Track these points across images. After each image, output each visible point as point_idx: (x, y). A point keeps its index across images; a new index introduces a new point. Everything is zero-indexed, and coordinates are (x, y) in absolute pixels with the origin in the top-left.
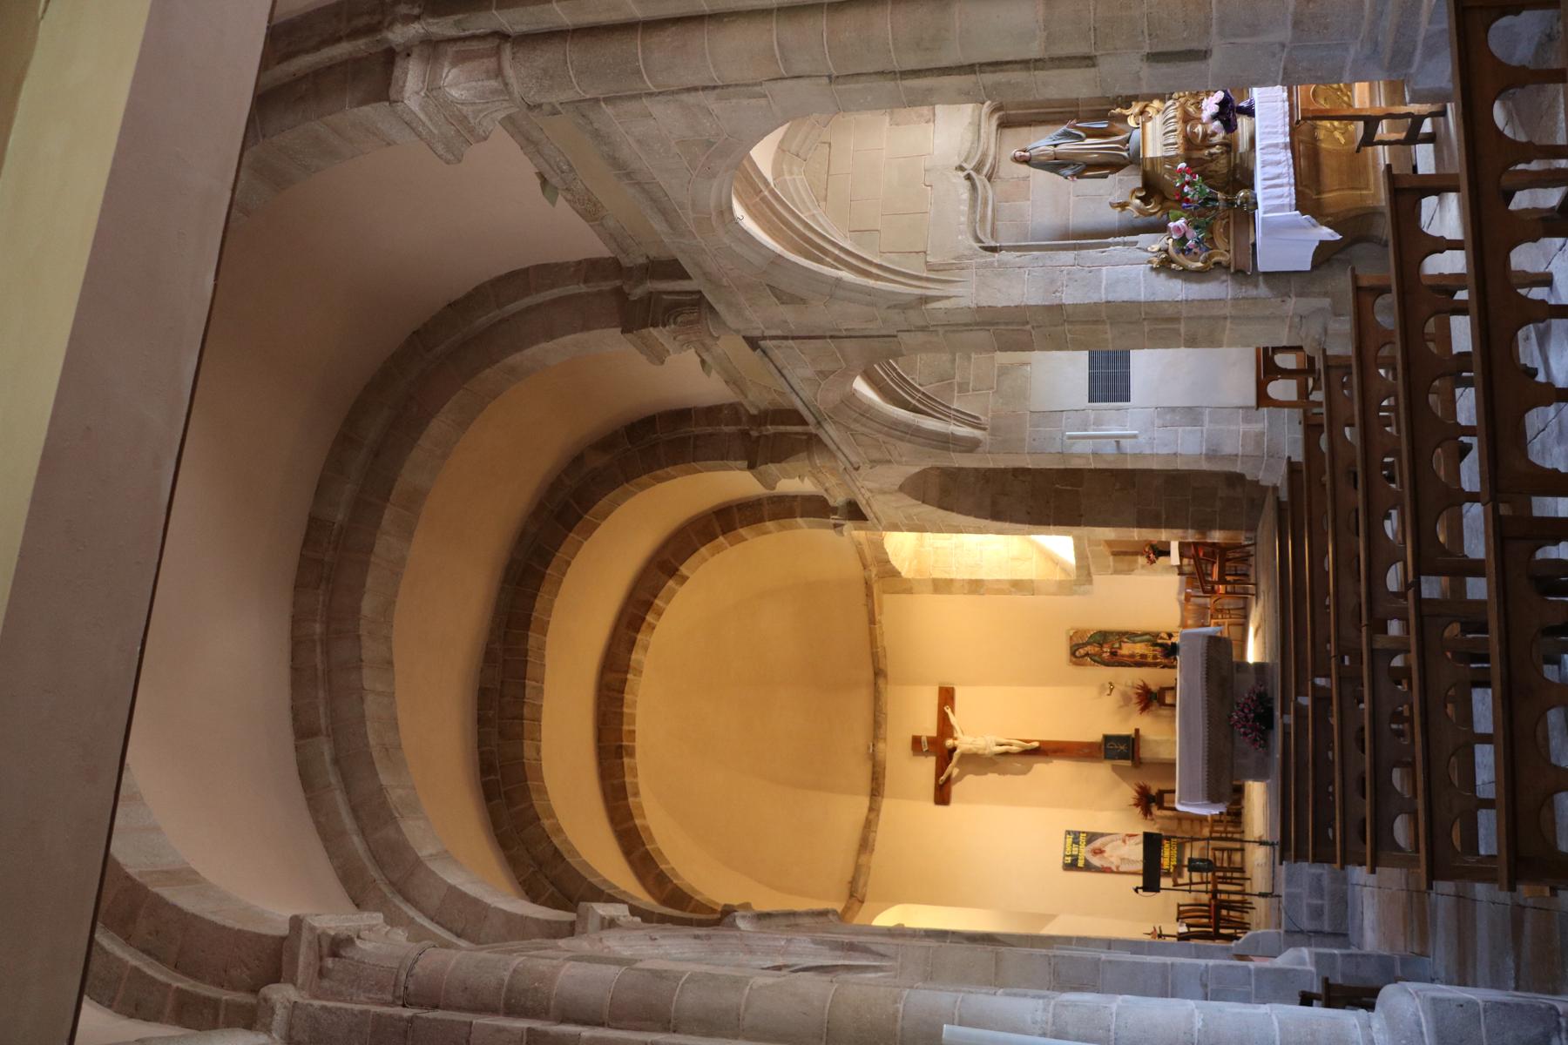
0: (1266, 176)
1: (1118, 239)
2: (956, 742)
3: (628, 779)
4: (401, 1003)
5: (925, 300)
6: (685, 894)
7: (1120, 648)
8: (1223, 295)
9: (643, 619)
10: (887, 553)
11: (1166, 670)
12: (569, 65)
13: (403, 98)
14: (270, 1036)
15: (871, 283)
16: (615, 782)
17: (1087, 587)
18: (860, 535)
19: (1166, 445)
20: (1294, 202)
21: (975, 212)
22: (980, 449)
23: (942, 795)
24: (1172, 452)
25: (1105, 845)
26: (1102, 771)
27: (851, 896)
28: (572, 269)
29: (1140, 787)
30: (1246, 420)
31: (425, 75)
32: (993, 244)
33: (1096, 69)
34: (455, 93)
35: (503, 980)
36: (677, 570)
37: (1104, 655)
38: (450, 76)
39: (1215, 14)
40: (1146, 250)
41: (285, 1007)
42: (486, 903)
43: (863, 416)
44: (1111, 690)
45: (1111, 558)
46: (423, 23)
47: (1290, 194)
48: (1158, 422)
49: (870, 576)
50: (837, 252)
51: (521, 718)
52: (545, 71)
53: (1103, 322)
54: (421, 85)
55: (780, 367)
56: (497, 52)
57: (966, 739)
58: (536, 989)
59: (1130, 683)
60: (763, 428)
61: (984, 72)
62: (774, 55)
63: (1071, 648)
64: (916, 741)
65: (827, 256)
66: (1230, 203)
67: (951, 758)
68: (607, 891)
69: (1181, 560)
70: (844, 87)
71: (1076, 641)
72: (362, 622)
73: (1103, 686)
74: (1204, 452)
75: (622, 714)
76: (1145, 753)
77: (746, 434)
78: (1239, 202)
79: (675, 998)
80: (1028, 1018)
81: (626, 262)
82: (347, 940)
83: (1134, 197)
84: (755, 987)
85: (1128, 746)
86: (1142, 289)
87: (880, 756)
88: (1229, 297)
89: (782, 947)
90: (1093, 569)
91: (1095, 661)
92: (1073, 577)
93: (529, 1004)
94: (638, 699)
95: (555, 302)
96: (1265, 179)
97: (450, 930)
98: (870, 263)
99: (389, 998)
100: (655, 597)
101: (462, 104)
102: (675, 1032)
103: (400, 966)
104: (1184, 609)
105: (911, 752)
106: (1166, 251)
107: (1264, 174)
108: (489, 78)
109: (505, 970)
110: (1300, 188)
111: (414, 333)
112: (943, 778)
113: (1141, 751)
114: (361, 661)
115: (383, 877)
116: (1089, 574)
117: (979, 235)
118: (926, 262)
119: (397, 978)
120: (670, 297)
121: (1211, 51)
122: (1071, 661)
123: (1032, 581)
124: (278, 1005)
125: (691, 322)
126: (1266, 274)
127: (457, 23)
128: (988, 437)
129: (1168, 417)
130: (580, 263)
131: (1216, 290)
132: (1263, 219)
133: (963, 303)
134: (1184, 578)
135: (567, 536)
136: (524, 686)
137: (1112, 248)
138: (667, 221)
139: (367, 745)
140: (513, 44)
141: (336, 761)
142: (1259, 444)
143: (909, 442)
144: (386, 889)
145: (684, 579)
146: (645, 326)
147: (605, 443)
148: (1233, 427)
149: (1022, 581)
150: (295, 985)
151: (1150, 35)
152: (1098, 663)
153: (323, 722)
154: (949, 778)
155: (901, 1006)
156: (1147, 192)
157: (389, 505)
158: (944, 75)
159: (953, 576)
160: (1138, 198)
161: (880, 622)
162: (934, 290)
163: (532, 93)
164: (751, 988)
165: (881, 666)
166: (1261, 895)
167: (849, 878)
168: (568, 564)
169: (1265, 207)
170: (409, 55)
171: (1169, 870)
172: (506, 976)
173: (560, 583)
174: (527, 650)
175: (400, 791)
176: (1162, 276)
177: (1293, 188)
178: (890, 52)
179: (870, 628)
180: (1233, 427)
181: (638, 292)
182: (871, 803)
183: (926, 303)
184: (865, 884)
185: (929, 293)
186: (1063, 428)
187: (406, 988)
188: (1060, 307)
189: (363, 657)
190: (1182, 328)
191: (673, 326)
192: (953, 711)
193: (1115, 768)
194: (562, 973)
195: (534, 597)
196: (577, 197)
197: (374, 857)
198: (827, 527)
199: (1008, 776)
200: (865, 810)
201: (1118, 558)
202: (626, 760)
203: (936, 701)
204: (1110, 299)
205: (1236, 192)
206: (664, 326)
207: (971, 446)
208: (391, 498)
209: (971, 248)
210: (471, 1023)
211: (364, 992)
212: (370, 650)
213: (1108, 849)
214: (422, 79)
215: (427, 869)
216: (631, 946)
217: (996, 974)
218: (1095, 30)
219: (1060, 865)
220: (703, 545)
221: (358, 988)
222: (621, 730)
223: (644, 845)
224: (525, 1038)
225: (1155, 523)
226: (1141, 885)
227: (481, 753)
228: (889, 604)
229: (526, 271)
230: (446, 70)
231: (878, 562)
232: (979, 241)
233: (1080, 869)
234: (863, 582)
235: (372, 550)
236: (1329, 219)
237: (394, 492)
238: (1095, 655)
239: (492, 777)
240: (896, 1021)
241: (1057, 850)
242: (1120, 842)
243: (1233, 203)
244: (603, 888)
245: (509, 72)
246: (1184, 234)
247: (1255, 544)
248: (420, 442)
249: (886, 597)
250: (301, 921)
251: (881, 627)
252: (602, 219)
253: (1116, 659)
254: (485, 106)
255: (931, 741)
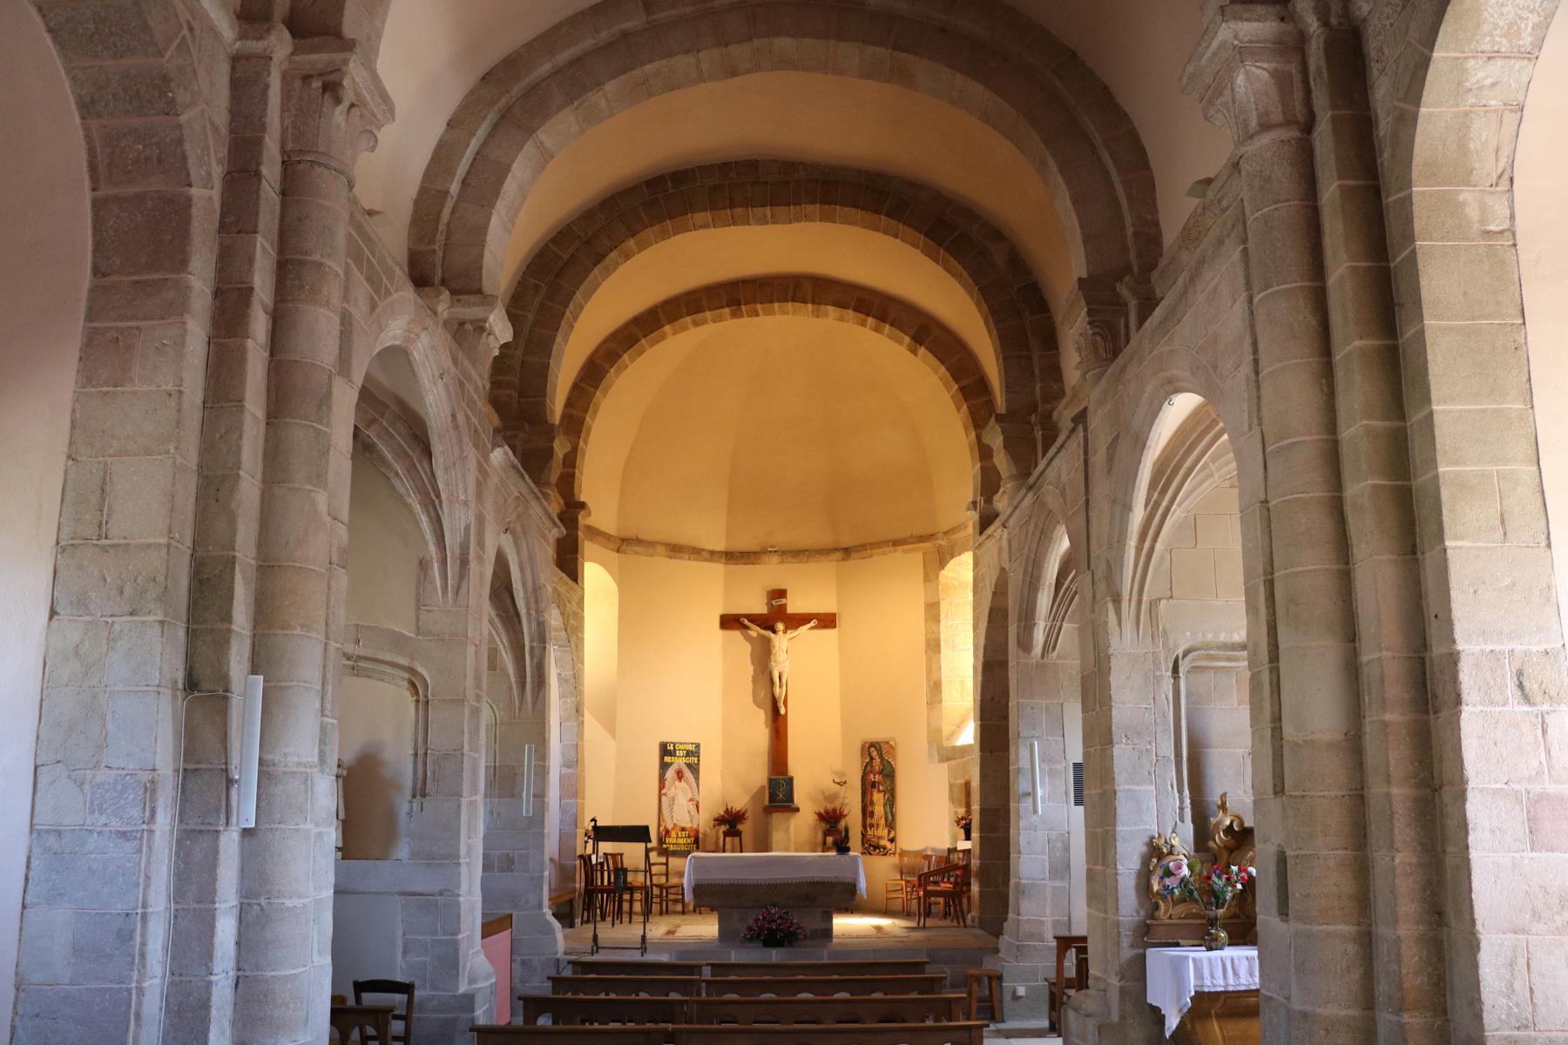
0: (1236, 961)
1: (1188, 801)
2: (781, 633)
3: (708, 314)
4: (285, 159)
5: (1117, 600)
6: (601, 381)
7: (879, 791)
8: (1122, 911)
9: (868, 315)
10: (960, 554)
11: (860, 836)
12: (1274, 207)
13: (1227, 21)
14: (236, 40)
15: (1132, 543)
16: (704, 302)
17: (936, 758)
18: (970, 529)
19: (1028, 843)
20: (1206, 990)
21: (1219, 648)
22: (1021, 653)
23: (730, 622)
24: (1022, 850)
25: (687, 782)
26: (759, 776)
27: (623, 540)
28: (1149, 217)
29: (744, 814)
30: (1056, 924)
31: (1260, 42)
32: (1181, 669)
33: (1272, 796)
34: (1240, 79)
35: (310, 255)
36: (921, 345)
37: (872, 776)
38: (1258, 72)
39: (1315, 928)
40: (1173, 832)
41: (265, 50)
42: (495, 204)
43: (1041, 534)
44: (838, 783)
45: (963, 781)
46: (1319, 31)
47: (1215, 986)
48: (1053, 835)
49: (937, 539)
50: (1164, 504)
51: (732, 207)
52: (1269, 179)
53: (1101, 787)
54: (1246, 39)
55: (1066, 446)
56: (1289, 122)
57: (782, 641)
58: (303, 287)
59: (846, 801)
60: (1039, 427)
61: (1270, 673)
62: (1283, 439)
63: (877, 743)
64: (781, 593)
65: (1159, 493)
66: (1213, 922)
67: (766, 628)
68: (568, 310)
69: (961, 851)
70: (1258, 516)
71: (884, 747)
72: (766, 40)
73: (842, 775)
74: (1023, 881)
75: (772, 302)
76: (776, 818)
77: (1034, 409)
78: (1213, 931)
79: (298, 421)
80: (290, 749)
81: (1155, 274)
82: (338, 98)
83: (1232, 818)
84: (312, 494)
85: (783, 801)
86: (1130, 828)
87: (766, 558)
88: (1120, 918)
89: (458, 497)
90: (953, 762)
91: (866, 767)
92: (946, 744)
93: (288, 283)
94: (790, 316)
95: (1115, 202)
96: (1232, 960)
97: (469, 172)
98: (1155, 539)
99: (289, 146)
100: (892, 325)
101: (1232, 89)
102: (267, 424)
103: (319, 153)
104: (916, 854)
105: (770, 589)
106: (1171, 853)
107: (1239, 959)
108: (1259, 117)
109: (322, 255)
110: (1223, 997)
111: (1074, 52)
112: (746, 622)
113: (778, 814)
114: (726, 46)
115: (513, 100)
116: (948, 759)
117: (1191, 654)
118: (1160, 600)
119: (309, 152)
120: (1122, 326)
121: (1287, 921)
122: (865, 743)
123: (940, 702)
124: (265, 43)
125: (1096, 351)
126: (1144, 956)
127: (1319, 69)
128: (1034, 661)
129: (1059, 845)
130: (1157, 224)
131: (1128, 905)
132: (1187, 957)
133: (1114, 641)
134: (946, 854)
135: (920, 233)
136: (763, 205)
137: (1177, 795)
138: (1161, 323)
139: (643, 64)
140: (1300, 139)
141: (625, 34)
142: (1031, 936)
143: (1023, 581)
144: (503, 102)
145: (914, 352)
146: (1088, 303)
147: (1018, 262)
148: (1048, 910)
149: (941, 692)
150: (292, 54)
151: (1297, 856)
152: (865, 770)
153: (661, 16)
154: (746, 627)
155: (298, 631)
156: (1238, 832)
157: (890, 51)
158: (1269, 628)
159: (942, 622)
160: (1232, 822)
161: (895, 551)
162: (1128, 609)
163: (1248, 167)
164: (311, 491)
165: (853, 555)
166: (595, 938)
167: (641, 537)
168: (896, 236)
169: (1201, 960)
170: (1282, 19)
171: (665, 843)
172: (316, 257)
173: (876, 229)
174: (800, 204)
175: (603, 103)
176: (1144, 849)
177: (1222, 989)
178: (1286, 569)
179: (888, 541)
180: (1048, 910)
181: (1124, 291)
182: (718, 552)
183: (1114, 601)
184: (635, 553)
185: (1125, 604)
186: (1045, 737)
187: (299, 162)
188: (1111, 743)
189: (731, 48)
190: (1098, 868)
191: (1091, 332)
192: (812, 628)
193: (762, 788)
194: (322, 310)
195: (855, 205)
196: (1199, 219)
197: (533, 88)
198: (975, 495)
199: (751, 686)
200: (711, 548)
201: (964, 787)
202: (727, 310)
203: (821, 611)
204: (1119, 794)
205: (1225, 927)
206: (1089, 323)
207: (1025, 644)
208: (896, 52)
209: (1177, 646)
210: (256, 232)
211: (293, 122)
212: (739, 52)
213: (683, 784)
214: (1254, 39)
215: (525, 141)
216: (427, 356)
217: (444, 700)
218: (1303, 797)
219: (665, 740)
220: (948, 369)
221: (295, 116)
222: (755, 303)
223: (645, 336)
224: (244, 286)
225: (983, 828)
226: (598, 824)
227: (693, 171)
228: (911, 560)
229: (1147, 166)
230: (1265, 65)
231: (952, 547)
232: (1185, 656)
233: (662, 759)
234: (932, 532)
235: (841, 40)
236: (1189, 1026)
237: (904, 54)
238: (872, 767)
239: (670, 184)
240: (282, 629)
241: (679, 735)
242: (690, 796)
243: (1212, 925)
244: (571, 306)
245: (1266, 139)
246: (1174, 875)
247: (965, 926)
248: (958, 74)
249: (920, 556)
250: (351, 51)
251: (891, 552)
252: (1187, 248)
253: (869, 787)
254: (1233, 115)
255: (783, 607)
